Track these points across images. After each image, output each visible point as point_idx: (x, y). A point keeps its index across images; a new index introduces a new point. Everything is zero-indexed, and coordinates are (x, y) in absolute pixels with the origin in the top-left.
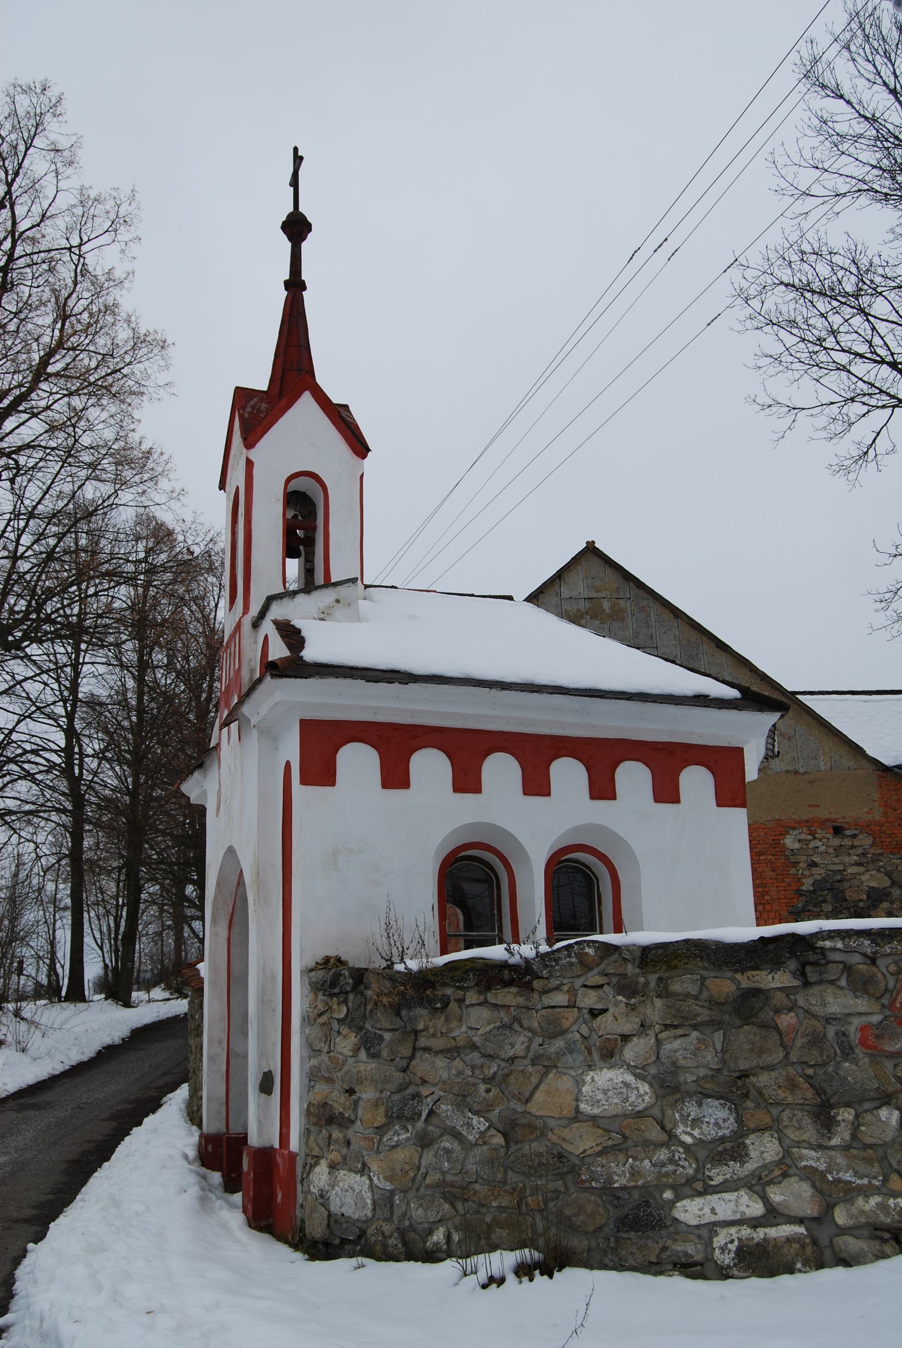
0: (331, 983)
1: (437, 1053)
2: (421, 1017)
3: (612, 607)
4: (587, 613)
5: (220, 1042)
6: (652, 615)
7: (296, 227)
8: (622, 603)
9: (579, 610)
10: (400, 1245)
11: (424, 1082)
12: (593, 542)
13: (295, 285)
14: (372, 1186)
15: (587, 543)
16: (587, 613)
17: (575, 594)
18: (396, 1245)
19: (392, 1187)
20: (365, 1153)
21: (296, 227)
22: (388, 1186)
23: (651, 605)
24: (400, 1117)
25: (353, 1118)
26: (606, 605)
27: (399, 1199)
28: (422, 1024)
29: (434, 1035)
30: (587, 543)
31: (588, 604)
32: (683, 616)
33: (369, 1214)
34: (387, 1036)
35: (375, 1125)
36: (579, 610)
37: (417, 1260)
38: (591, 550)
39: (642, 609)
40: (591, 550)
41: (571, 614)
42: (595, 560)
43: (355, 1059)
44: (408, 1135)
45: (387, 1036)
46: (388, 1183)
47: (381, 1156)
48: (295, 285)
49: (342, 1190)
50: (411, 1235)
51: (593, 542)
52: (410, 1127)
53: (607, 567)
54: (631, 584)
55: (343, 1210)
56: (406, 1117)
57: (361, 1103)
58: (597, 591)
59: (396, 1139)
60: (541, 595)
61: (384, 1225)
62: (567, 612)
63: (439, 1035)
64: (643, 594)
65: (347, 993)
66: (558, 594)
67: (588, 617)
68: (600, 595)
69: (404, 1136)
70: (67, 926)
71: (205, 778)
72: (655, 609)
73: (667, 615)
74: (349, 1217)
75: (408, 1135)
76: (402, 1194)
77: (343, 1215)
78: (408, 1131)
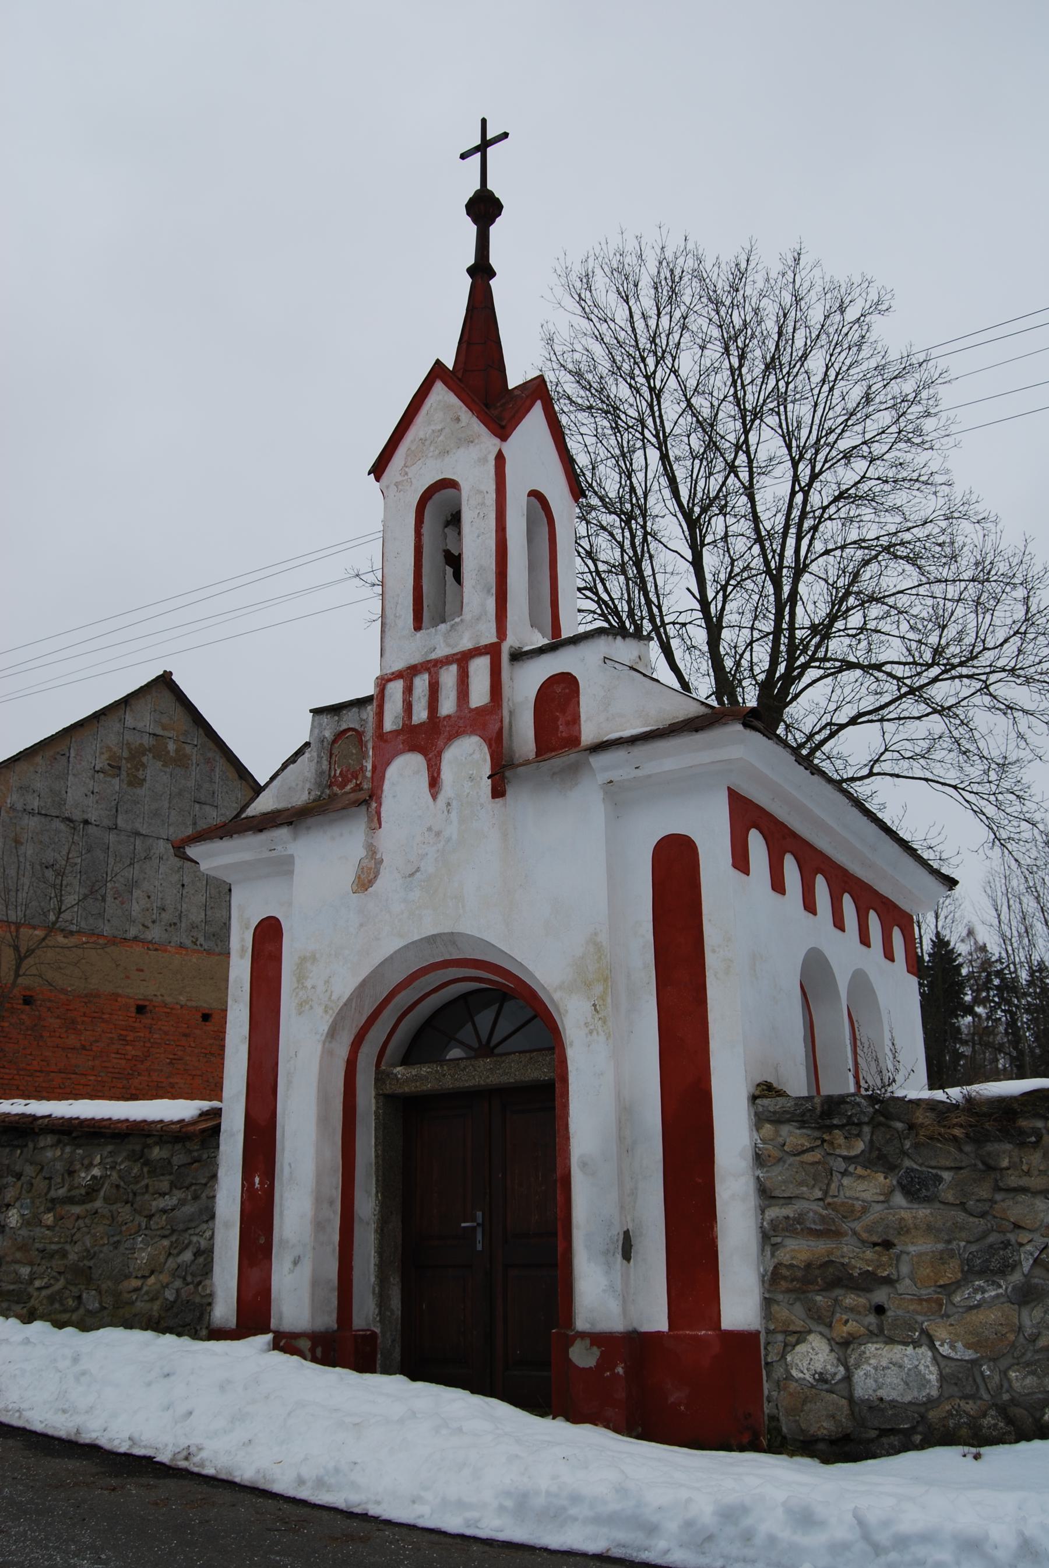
0: (822, 1112)
1: (1035, 1193)
2: (1004, 1153)
3: (177, 751)
4: (150, 750)
5: (331, 1203)
6: (217, 770)
7: (484, 208)
8: (188, 749)
9: (141, 745)
10: (1001, 1424)
11: (1017, 1226)
12: (171, 673)
13: (481, 271)
14: (938, 1358)
15: (165, 671)
16: (150, 750)
17: (140, 725)
18: (995, 1425)
19: (974, 1356)
20: (920, 1318)
21: (484, 208)
22: (969, 1355)
23: (217, 758)
24: (982, 1273)
25: (895, 1277)
26: (171, 747)
27: (989, 1368)
28: (1007, 1160)
29: (1028, 1173)
30: (165, 671)
31: (152, 741)
32: (250, 781)
33: (935, 1393)
34: (947, 1176)
35: (941, 1283)
36: (141, 745)
37: (1029, 1439)
38: (165, 682)
39: (208, 761)
40: (165, 682)
41: (133, 746)
42: (167, 695)
43: (886, 1205)
44: (1000, 1291)
45: (947, 1176)
46: (970, 1352)
47: (952, 1320)
48: (481, 271)
49: (876, 1368)
50: (1017, 1412)
51: (171, 673)
52: (1002, 1282)
53: (178, 704)
54: (200, 730)
55: (881, 1393)
56: (992, 1271)
57: (904, 1257)
58: (164, 729)
59: (979, 1297)
60: (102, 717)
61: (962, 1403)
62: (128, 744)
63: (1036, 1173)
64: (211, 744)
65: (859, 1124)
66: (122, 721)
67: (151, 755)
68: (166, 734)
69: (993, 1293)
70: (331, 1012)
71: (295, 839)
72: (221, 763)
73: (232, 774)
74: (892, 1401)
75: (1000, 1291)
76: (991, 1364)
77: (881, 1399)
78: (1001, 1287)
